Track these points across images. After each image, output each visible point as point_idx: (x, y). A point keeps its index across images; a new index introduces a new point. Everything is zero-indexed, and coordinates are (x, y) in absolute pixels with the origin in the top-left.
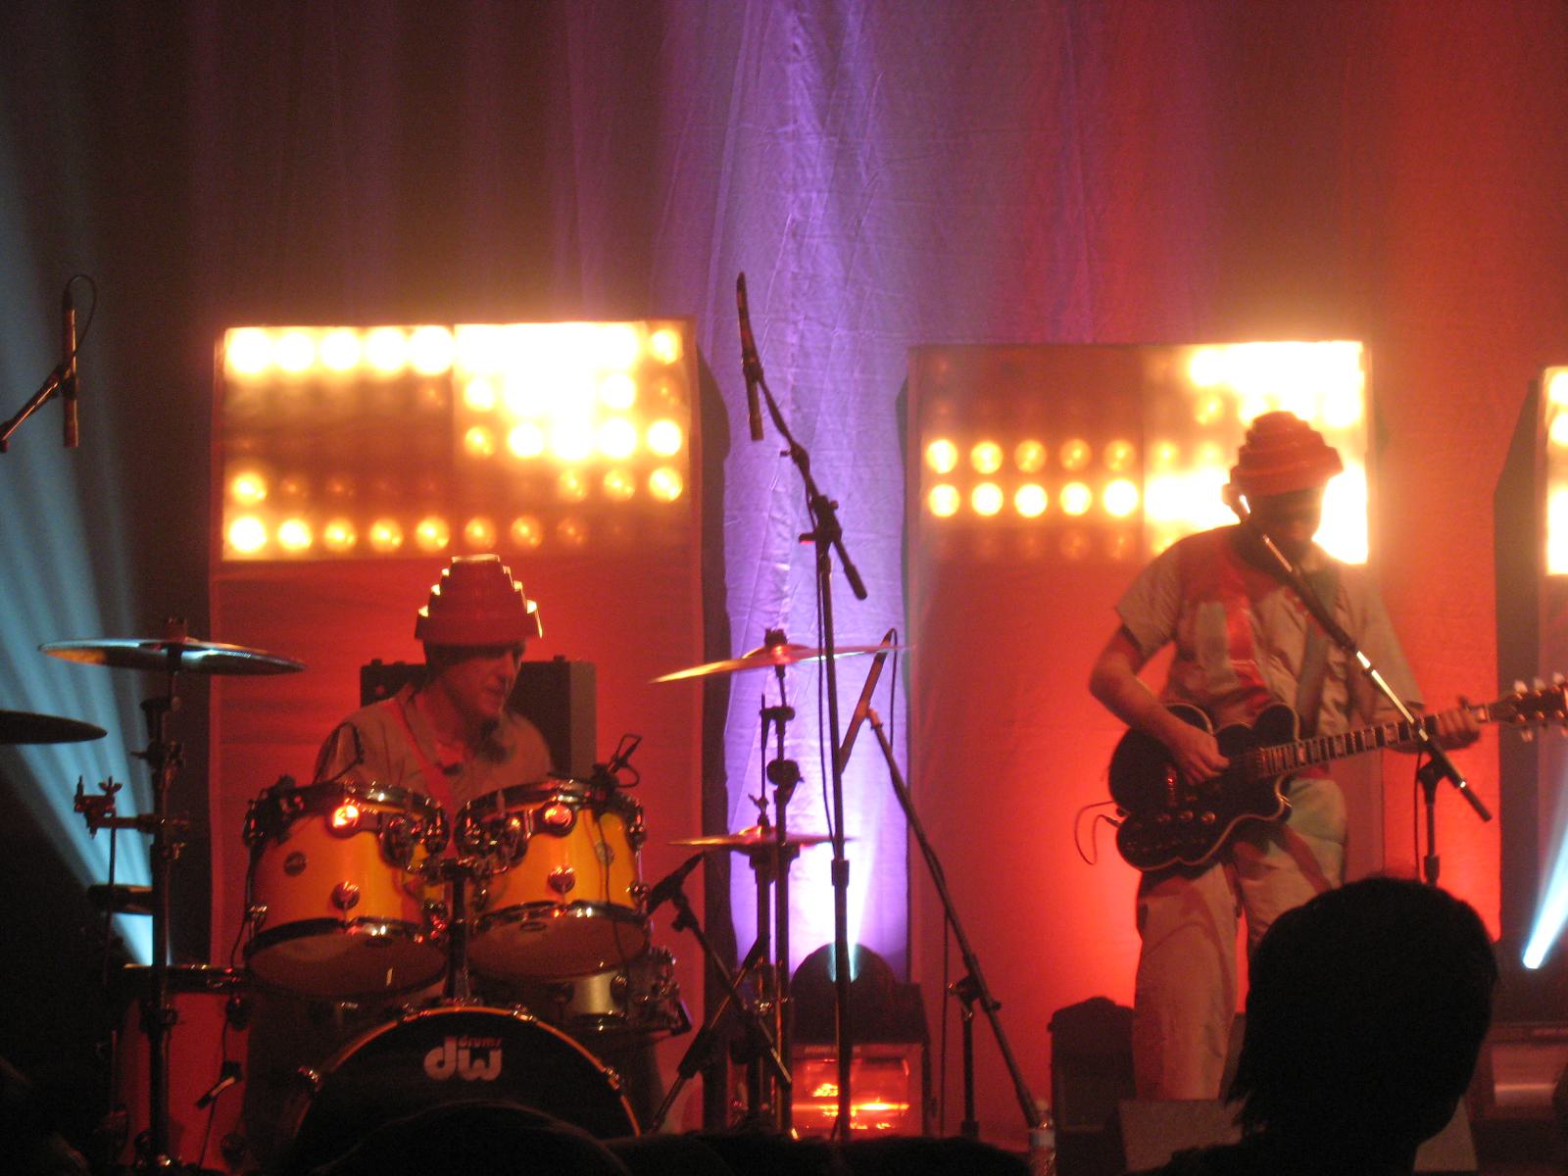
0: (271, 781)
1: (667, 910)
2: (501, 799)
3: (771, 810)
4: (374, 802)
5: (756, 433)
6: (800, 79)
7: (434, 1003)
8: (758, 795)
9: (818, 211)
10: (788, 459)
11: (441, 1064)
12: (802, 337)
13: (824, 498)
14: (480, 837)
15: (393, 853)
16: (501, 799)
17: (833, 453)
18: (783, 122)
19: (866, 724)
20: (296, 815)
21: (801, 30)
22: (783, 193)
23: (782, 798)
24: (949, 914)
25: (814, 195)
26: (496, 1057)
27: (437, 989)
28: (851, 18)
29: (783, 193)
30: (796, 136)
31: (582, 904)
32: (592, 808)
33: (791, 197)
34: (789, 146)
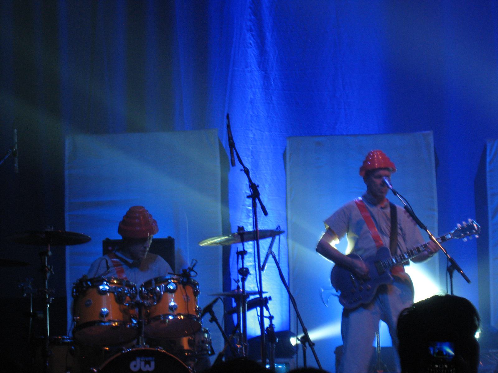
0: (80, 277)
1: (208, 316)
2: (153, 282)
3: (240, 284)
4: (114, 283)
5: (233, 164)
6: (252, 53)
7: (133, 347)
8: (236, 280)
9: (259, 95)
10: (243, 172)
11: (135, 366)
12: (254, 135)
13: (254, 184)
14: (147, 294)
15: (119, 299)
16: (153, 282)
17: (265, 172)
18: (247, 67)
19: (271, 256)
20: (88, 287)
21: (252, 38)
22: (247, 90)
23: (244, 280)
24: (298, 316)
25: (257, 90)
26: (153, 364)
27: (135, 342)
28: (268, 34)
29: (247, 90)
30: (251, 72)
31: (180, 315)
32: (182, 284)
33: (250, 91)
34: (248, 75)
